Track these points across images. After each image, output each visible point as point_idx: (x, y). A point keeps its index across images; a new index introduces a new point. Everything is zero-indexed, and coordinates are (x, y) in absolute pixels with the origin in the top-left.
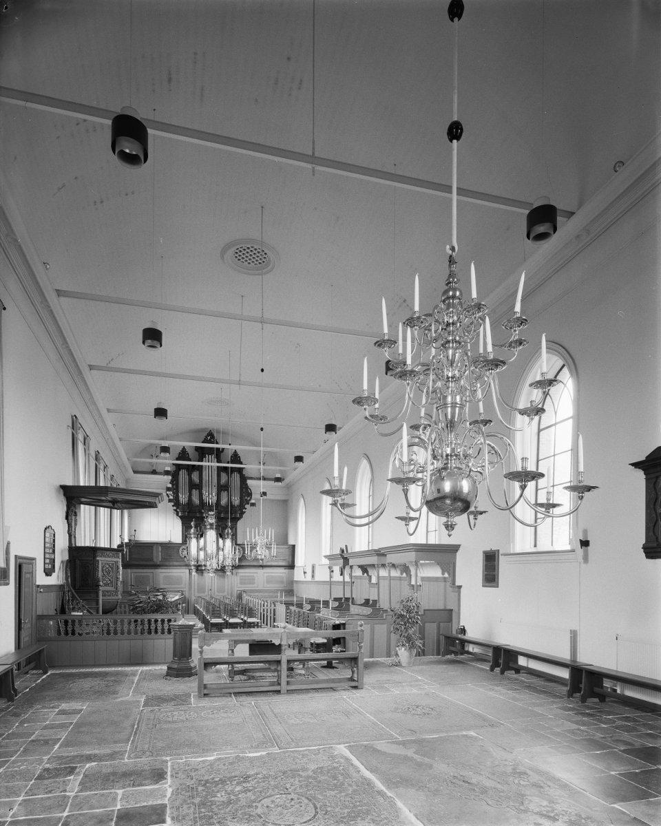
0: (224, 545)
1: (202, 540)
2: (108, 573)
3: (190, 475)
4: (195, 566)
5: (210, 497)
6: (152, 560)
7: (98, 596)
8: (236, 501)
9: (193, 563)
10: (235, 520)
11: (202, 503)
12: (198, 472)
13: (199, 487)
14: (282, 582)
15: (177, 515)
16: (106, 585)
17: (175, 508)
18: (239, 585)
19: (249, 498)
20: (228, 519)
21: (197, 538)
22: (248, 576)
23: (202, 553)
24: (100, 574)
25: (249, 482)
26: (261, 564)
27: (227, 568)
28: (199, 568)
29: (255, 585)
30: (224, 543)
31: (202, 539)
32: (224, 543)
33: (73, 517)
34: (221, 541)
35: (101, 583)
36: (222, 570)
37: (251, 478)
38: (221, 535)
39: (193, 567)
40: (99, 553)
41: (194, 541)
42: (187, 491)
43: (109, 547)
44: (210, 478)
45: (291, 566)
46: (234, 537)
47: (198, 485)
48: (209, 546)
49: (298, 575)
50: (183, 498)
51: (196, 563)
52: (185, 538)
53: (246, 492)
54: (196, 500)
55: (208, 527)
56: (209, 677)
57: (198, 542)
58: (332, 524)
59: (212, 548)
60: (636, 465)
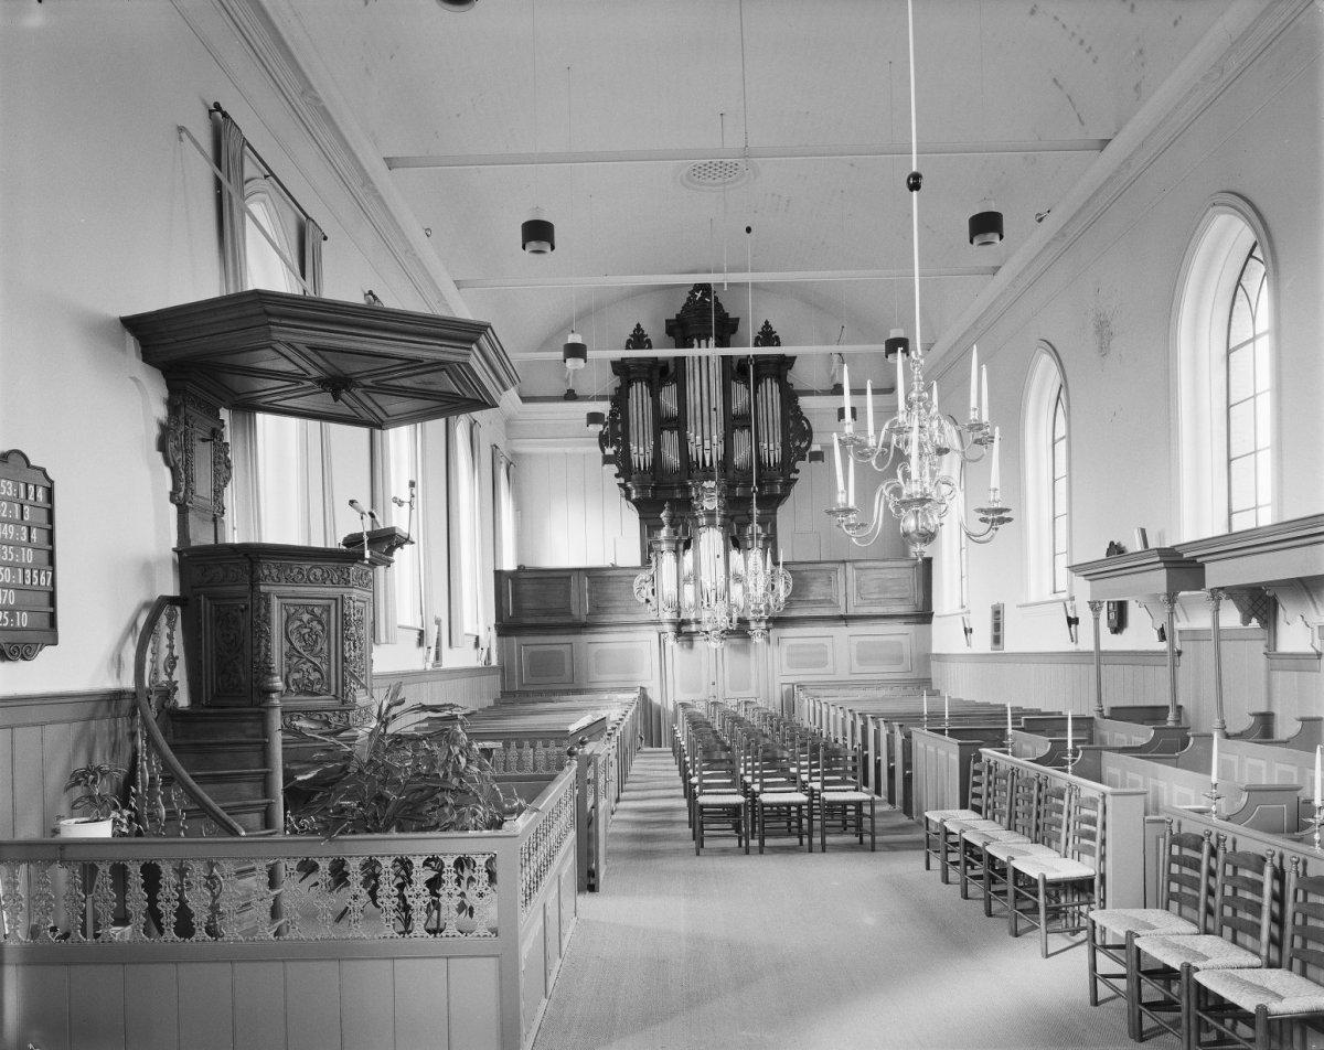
1: (688, 557)
3: (655, 395)
5: (706, 443)
11: (691, 467)
13: (678, 423)
14: (900, 659)
15: (628, 497)
17: (622, 480)
19: (804, 445)
20: (754, 499)
21: (676, 552)
23: (689, 592)
26: (842, 612)
27: (753, 625)
28: (684, 629)
29: (829, 668)
31: (689, 554)
35: (278, 683)
38: (736, 541)
41: (668, 560)
48: (715, 571)
50: (641, 453)
54: (672, 457)
55: (703, 521)
57: (678, 561)
59: (712, 574)
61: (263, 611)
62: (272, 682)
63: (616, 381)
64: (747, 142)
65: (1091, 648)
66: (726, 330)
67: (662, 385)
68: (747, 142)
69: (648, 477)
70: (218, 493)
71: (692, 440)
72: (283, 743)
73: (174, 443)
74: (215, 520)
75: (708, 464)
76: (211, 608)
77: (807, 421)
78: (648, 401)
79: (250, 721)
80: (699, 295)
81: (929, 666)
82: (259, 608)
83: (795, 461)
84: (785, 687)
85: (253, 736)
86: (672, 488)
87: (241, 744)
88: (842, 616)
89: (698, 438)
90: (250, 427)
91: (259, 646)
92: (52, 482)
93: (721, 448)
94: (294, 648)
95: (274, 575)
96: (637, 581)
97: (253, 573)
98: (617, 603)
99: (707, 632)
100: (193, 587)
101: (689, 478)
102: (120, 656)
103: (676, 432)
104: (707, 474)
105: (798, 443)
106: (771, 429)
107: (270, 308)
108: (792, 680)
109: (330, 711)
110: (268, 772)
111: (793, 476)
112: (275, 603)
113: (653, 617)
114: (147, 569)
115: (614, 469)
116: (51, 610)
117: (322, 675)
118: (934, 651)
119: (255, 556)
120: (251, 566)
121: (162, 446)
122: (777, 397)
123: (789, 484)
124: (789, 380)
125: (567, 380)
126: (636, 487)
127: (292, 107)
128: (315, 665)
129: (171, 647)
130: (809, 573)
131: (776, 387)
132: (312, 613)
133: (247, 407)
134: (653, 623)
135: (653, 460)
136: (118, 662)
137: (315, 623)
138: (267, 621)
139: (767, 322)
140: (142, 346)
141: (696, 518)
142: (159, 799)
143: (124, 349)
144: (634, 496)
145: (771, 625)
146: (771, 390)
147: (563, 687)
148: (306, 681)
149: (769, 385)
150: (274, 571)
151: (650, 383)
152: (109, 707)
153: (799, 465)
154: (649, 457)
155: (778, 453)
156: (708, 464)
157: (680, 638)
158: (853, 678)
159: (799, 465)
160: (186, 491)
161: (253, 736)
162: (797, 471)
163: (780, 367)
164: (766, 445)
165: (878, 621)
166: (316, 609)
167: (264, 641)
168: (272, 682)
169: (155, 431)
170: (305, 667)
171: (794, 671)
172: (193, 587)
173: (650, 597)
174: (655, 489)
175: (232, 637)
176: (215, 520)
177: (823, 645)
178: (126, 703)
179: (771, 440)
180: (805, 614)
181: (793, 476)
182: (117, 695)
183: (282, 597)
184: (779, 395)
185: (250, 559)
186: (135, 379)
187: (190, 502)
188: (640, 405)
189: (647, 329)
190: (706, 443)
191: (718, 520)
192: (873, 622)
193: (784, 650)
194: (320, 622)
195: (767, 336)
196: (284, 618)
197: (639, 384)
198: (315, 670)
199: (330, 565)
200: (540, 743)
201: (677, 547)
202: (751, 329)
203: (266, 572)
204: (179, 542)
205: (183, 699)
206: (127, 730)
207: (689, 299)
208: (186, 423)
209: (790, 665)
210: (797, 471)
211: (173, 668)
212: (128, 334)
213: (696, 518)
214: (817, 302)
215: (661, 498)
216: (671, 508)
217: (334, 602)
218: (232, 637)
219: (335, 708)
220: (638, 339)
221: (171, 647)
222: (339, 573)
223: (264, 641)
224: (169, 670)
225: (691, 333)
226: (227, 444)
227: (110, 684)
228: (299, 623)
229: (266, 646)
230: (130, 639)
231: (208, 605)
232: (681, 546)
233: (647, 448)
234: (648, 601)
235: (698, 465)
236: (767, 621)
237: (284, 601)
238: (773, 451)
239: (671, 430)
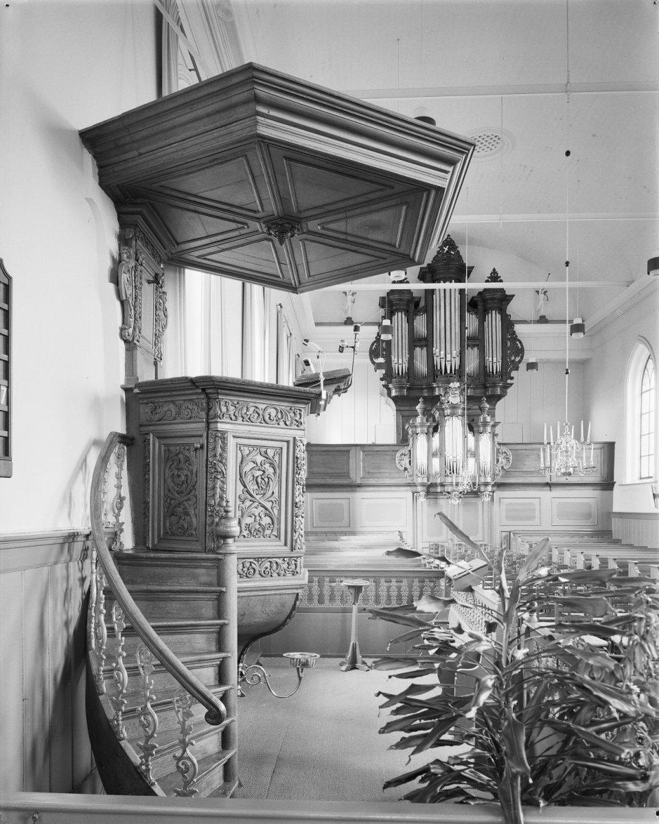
0: (477, 446)
2: (263, 483)
3: (410, 322)
5: (447, 354)
6: (347, 476)
7: (221, 580)
8: (495, 361)
11: (435, 372)
12: (425, 316)
15: (389, 394)
16: (254, 532)
17: (383, 383)
18: (505, 522)
19: (517, 359)
22: (523, 504)
23: (436, 462)
24: (232, 489)
25: (518, 328)
26: (548, 480)
28: (432, 490)
29: (537, 521)
30: (477, 441)
31: (437, 435)
32: (477, 441)
33: (148, 290)
35: (234, 527)
36: (474, 493)
37: (524, 322)
38: (473, 426)
39: (420, 489)
40: (226, 404)
41: (421, 441)
42: (406, 351)
43: (274, 382)
44: (448, 324)
45: (607, 484)
47: (425, 339)
49: (621, 502)
50: (399, 362)
51: (425, 480)
52: (404, 439)
53: (513, 348)
54: (421, 366)
55: (448, 412)
61: (219, 450)
62: (230, 527)
64: (568, 79)
66: (460, 272)
67: (416, 315)
68: (568, 79)
69: (404, 380)
70: (157, 336)
71: (438, 354)
72: (238, 592)
74: (156, 364)
75: (449, 372)
76: (160, 448)
77: (521, 343)
78: (405, 325)
79: (204, 567)
80: (446, 249)
81: (611, 522)
82: (215, 448)
84: (504, 534)
85: (205, 584)
86: (423, 389)
87: (197, 592)
88: (547, 483)
89: (443, 352)
90: (180, 287)
91: (214, 488)
92: (9, 278)
93: (458, 360)
94: (248, 491)
95: (232, 413)
96: (398, 454)
97: (209, 409)
98: (383, 470)
99: (449, 493)
100: (141, 426)
101: (434, 382)
102: (71, 494)
103: (425, 349)
104: (448, 378)
105: (513, 358)
106: (494, 348)
107: (262, 92)
108: (509, 529)
109: (279, 558)
110: (224, 625)
111: (509, 381)
112: (232, 443)
113: (409, 480)
114: (97, 404)
116: (5, 434)
118: (616, 509)
119: (208, 390)
120: (208, 404)
125: (346, 312)
126: (395, 388)
128: (266, 509)
129: (119, 487)
130: (523, 452)
131: (499, 317)
132: (265, 455)
133: (179, 262)
134: (409, 485)
135: (408, 369)
136: (68, 498)
137: (267, 466)
138: (223, 460)
139: (494, 270)
140: (100, 167)
141: (443, 410)
142: (121, 660)
144: (394, 393)
145: (495, 488)
146: (494, 320)
147: (341, 529)
148: (258, 526)
149: (494, 315)
150: (232, 408)
151: (407, 312)
152: (62, 549)
153: (513, 374)
154: (405, 366)
155: (499, 365)
156: (449, 372)
157: (429, 496)
158: (556, 528)
159: (513, 374)
160: (134, 328)
161: (205, 584)
162: (512, 378)
164: (490, 358)
165: (573, 487)
166: (269, 451)
167: (219, 482)
168: (230, 527)
169: (108, 264)
170: (256, 512)
171: (509, 523)
172: (141, 426)
173: (408, 466)
174: (409, 389)
175: (183, 478)
176: (156, 364)
177: (533, 504)
178: (78, 546)
179: (495, 355)
180: (520, 480)
181: (509, 381)
182: (72, 537)
185: (207, 394)
186: (89, 200)
187: (138, 341)
188: (400, 328)
190: (447, 354)
191: (460, 411)
192: (569, 488)
193: (503, 507)
194: (272, 465)
195: (494, 277)
196: (239, 460)
197: (400, 314)
199: (284, 406)
200: (383, 580)
201: (428, 430)
203: (224, 409)
204: (127, 380)
205: (127, 542)
206: (79, 575)
207: (438, 252)
208: (137, 260)
209: (508, 518)
210: (512, 378)
211: (120, 509)
212: (85, 150)
213: (443, 410)
214: (530, 258)
215: (414, 394)
216: (424, 402)
217: (286, 443)
218: (183, 478)
219: (285, 555)
221: (119, 487)
222: (292, 415)
223: (219, 482)
224: (116, 511)
225: (438, 277)
227: (65, 526)
228: (252, 465)
229: (222, 489)
230: (81, 476)
231: (157, 445)
232: (431, 430)
233: (404, 359)
234: (406, 469)
235: (441, 372)
236: (493, 486)
237: (240, 441)
238: (495, 361)
239: (421, 347)
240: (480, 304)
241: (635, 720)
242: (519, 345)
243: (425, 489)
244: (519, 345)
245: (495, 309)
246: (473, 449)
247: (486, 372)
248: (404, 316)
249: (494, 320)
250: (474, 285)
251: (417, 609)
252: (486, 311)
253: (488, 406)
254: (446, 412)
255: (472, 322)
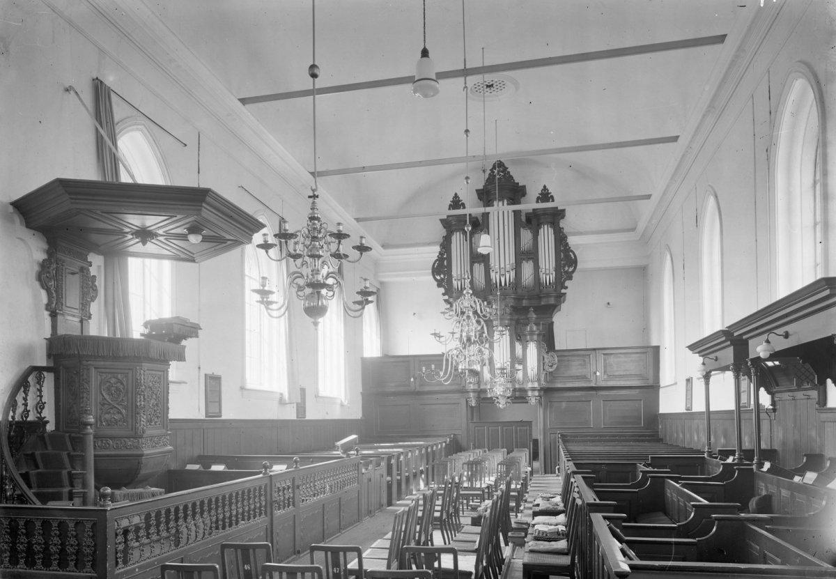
4: (474, 391)
9: (472, 387)
10: (551, 309)
17: (446, 297)
19: (571, 269)
27: (530, 393)
32: (524, 349)
34: (519, 347)
39: (472, 395)
46: (547, 340)
51: (476, 387)
53: (566, 260)
56: (699, 386)
58: (722, 262)
60: (692, 347)
63: (444, 232)
65: (703, 409)
66: (515, 193)
73: (49, 276)
75: (503, 284)
77: (574, 254)
83: (564, 281)
103: (483, 264)
111: (563, 291)
114: (26, 351)
115: (442, 290)
117: (123, 416)
121: (39, 278)
122: (552, 237)
123: (560, 297)
124: (561, 225)
127: (773, 22)
131: (551, 231)
137: (119, 384)
139: (545, 187)
143: (13, 222)
146: (547, 235)
153: (567, 283)
155: (552, 277)
156: (503, 284)
159: (567, 283)
160: (56, 303)
162: (566, 288)
163: (555, 217)
181: (563, 291)
183: (97, 368)
184: (553, 236)
189: (463, 197)
194: (122, 384)
195: (545, 196)
197: (458, 233)
198: (118, 413)
202: (533, 192)
210: (566, 288)
220: (456, 203)
226: (94, 276)
235: (497, 287)
239: (479, 262)
240: (532, 221)
241: (481, 502)
242: (572, 256)
243: (476, 394)
244: (572, 256)
245: (547, 223)
246: (521, 357)
247: (540, 283)
248: (462, 236)
249: (547, 235)
250: (529, 204)
251: (300, 401)
252: (539, 226)
253: (535, 316)
254: (494, 323)
255: (526, 235)
